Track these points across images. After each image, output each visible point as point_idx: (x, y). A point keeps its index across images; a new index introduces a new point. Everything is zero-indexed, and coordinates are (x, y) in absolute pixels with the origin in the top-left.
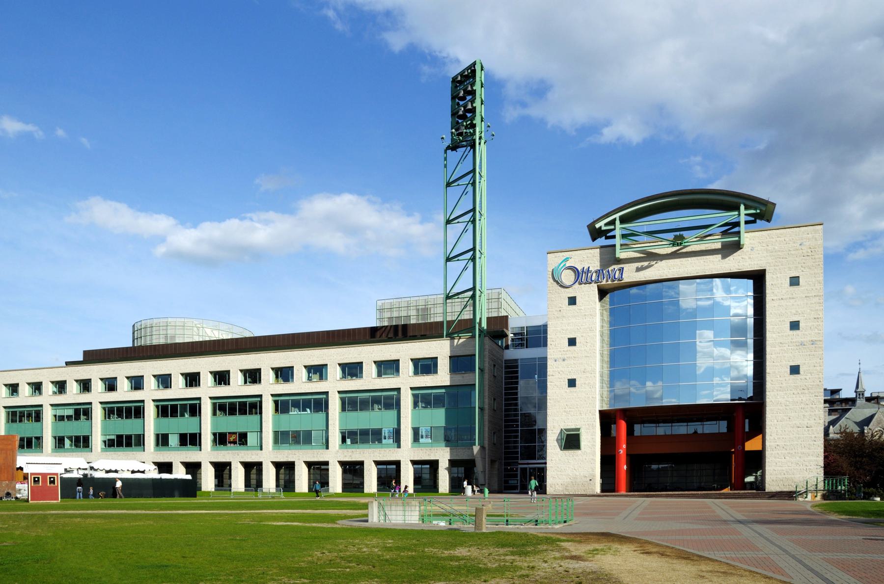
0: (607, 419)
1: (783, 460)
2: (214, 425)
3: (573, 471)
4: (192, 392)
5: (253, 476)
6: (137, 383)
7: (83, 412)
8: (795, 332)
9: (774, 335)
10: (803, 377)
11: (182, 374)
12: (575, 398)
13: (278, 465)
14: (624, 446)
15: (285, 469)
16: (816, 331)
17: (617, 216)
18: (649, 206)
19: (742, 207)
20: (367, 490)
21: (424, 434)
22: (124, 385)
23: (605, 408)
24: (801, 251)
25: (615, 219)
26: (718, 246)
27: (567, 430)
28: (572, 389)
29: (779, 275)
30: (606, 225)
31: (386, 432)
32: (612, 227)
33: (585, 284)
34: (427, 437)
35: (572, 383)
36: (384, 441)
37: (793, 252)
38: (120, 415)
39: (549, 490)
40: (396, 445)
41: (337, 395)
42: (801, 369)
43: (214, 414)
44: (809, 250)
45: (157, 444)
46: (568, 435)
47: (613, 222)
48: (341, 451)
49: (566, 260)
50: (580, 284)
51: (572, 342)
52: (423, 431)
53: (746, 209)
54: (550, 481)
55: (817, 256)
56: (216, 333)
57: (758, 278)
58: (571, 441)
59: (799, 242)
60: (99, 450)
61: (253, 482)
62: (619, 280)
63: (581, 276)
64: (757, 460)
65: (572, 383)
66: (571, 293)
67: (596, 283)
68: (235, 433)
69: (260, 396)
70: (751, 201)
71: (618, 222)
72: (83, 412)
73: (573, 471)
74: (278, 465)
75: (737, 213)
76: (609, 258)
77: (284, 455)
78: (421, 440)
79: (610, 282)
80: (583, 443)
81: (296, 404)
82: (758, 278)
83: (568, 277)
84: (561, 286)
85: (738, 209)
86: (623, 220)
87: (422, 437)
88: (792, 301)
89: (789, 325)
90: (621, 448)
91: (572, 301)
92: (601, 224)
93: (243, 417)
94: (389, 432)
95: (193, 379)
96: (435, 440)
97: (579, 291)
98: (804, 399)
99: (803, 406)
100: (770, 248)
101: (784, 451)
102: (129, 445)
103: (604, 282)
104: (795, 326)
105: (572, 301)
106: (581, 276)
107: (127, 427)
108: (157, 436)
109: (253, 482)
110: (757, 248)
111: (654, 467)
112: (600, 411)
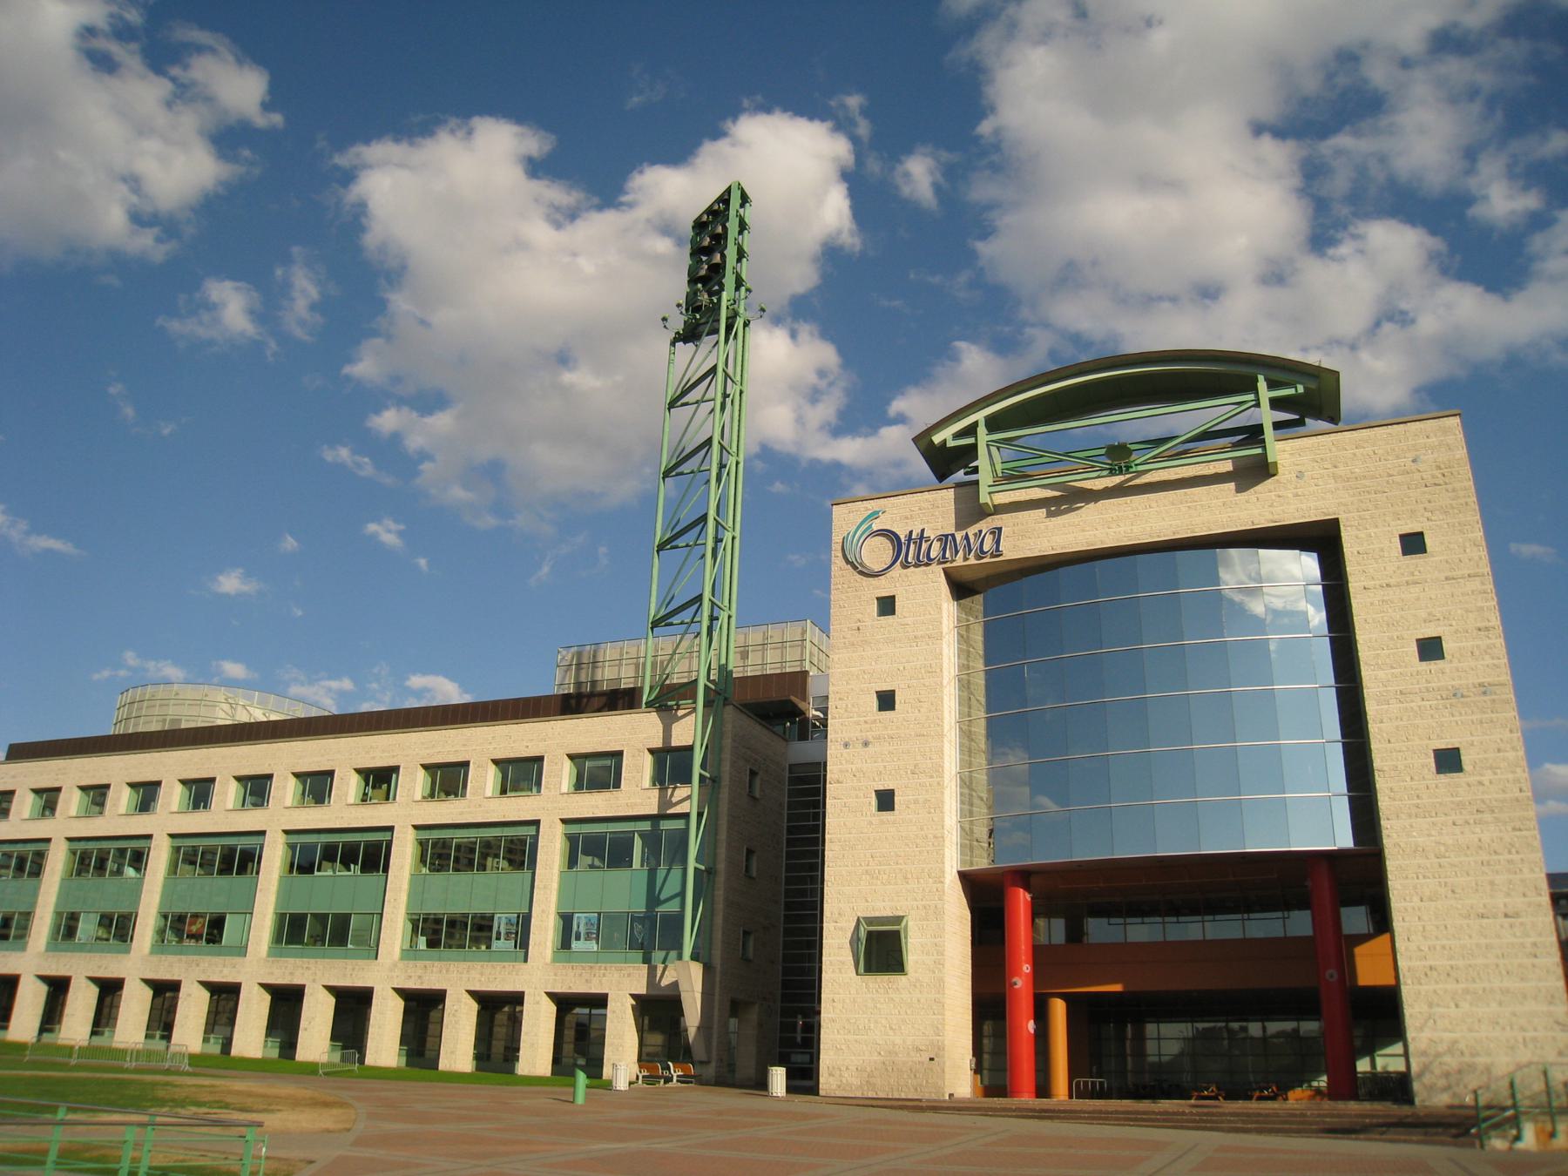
0: (985, 895)
1: (1453, 1010)
2: (167, 894)
3: (902, 1027)
4: (517, 807)
5: (500, 1031)
6: (257, 788)
7: (238, 859)
8: (1434, 665)
9: (1381, 674)
10: (1472, 779)
11: (358, 771)
12: (905, 836)
13: (564, 1003)
14: (1026, 968)
15: (423, 1009)
16: (1488, 661)
17: (980, 416)
18: (1183, 373)
19: (1262, 385)
20: (524, 1067)
21: (582, 930)
22: (227, 794)
23: (982, 863)
24: (1417, 476)
25: (976, 424)
26: (1227, 467)
27: (870, 921)
28: (886, 815)
29: (1372, 531)
30: (957, 436)
31: (500, 924)
32: (970, 441)
33: (916, 566)
34: (588, 938)
35: (886, 800)
36: (496, 945)
37: (1398, 479)
38: (207, 865)
39: (827, 1082)
40: (521, 954)
41: (560, 828)
42: (1466, 759)
43: (572, 861)
44: (1437, 473)
45: (278, 938)
46: (870, 934)
47: (971, 430)
48: (401, 965)
49: (875, 515)
50: (905, 566)
51: (886, 701)
52: (580, 923)
53: (1272, 385)
54: (827, 1059)
55: (1457, 485)
56: (945, 606)
57: (1322, 540)
58: (882, 950)
59: (1411, 456)
60: (549, 953)
61: (498, 1047)
62: (993, 556)
63: (906, 550)
64: (1381, 1013)
65: (886, 800)
66: (883, 587)
67: (940, 563)
68: (202, 915)
69: (537, 823)
70: (1280, 370)
71: (983, 435)
72: (238, 859)
73: (902, 1027)
74: (564, 1003)
75: (1252, 397)
76: (971, 510)
77: (288, 971)
78: (575, 945)
79: (972, 561)
80: (912, 957)
81: (329, 854)
82: (1322, 540)
83: (876, 553)
84: (861, 573)
85: (1255, 390)
86: (994, 424)
87: (578, 938)
88: (1416, 589)
89: (1414, 648)
90: (1018, 972)
91: (887, 606)
92: (944, 436)
93: (465, 877)
94: (509, 922)
95: (380, 779)
96: (608, 945)
97: (900, 583)
98: (1486, 837)
99: (1486, 857)
100: (1342, 470)
101: (1451, 986)
102: (318, 939)
103: (959, 561)
104: (1430, 649)
105: (887, 606)
106: (906, 550)
107: (462, 893)
108: (281, 917)
109: (498, 1047)
110: (1309, 474)
111: (1255, 1029)
112: (964, 877)
